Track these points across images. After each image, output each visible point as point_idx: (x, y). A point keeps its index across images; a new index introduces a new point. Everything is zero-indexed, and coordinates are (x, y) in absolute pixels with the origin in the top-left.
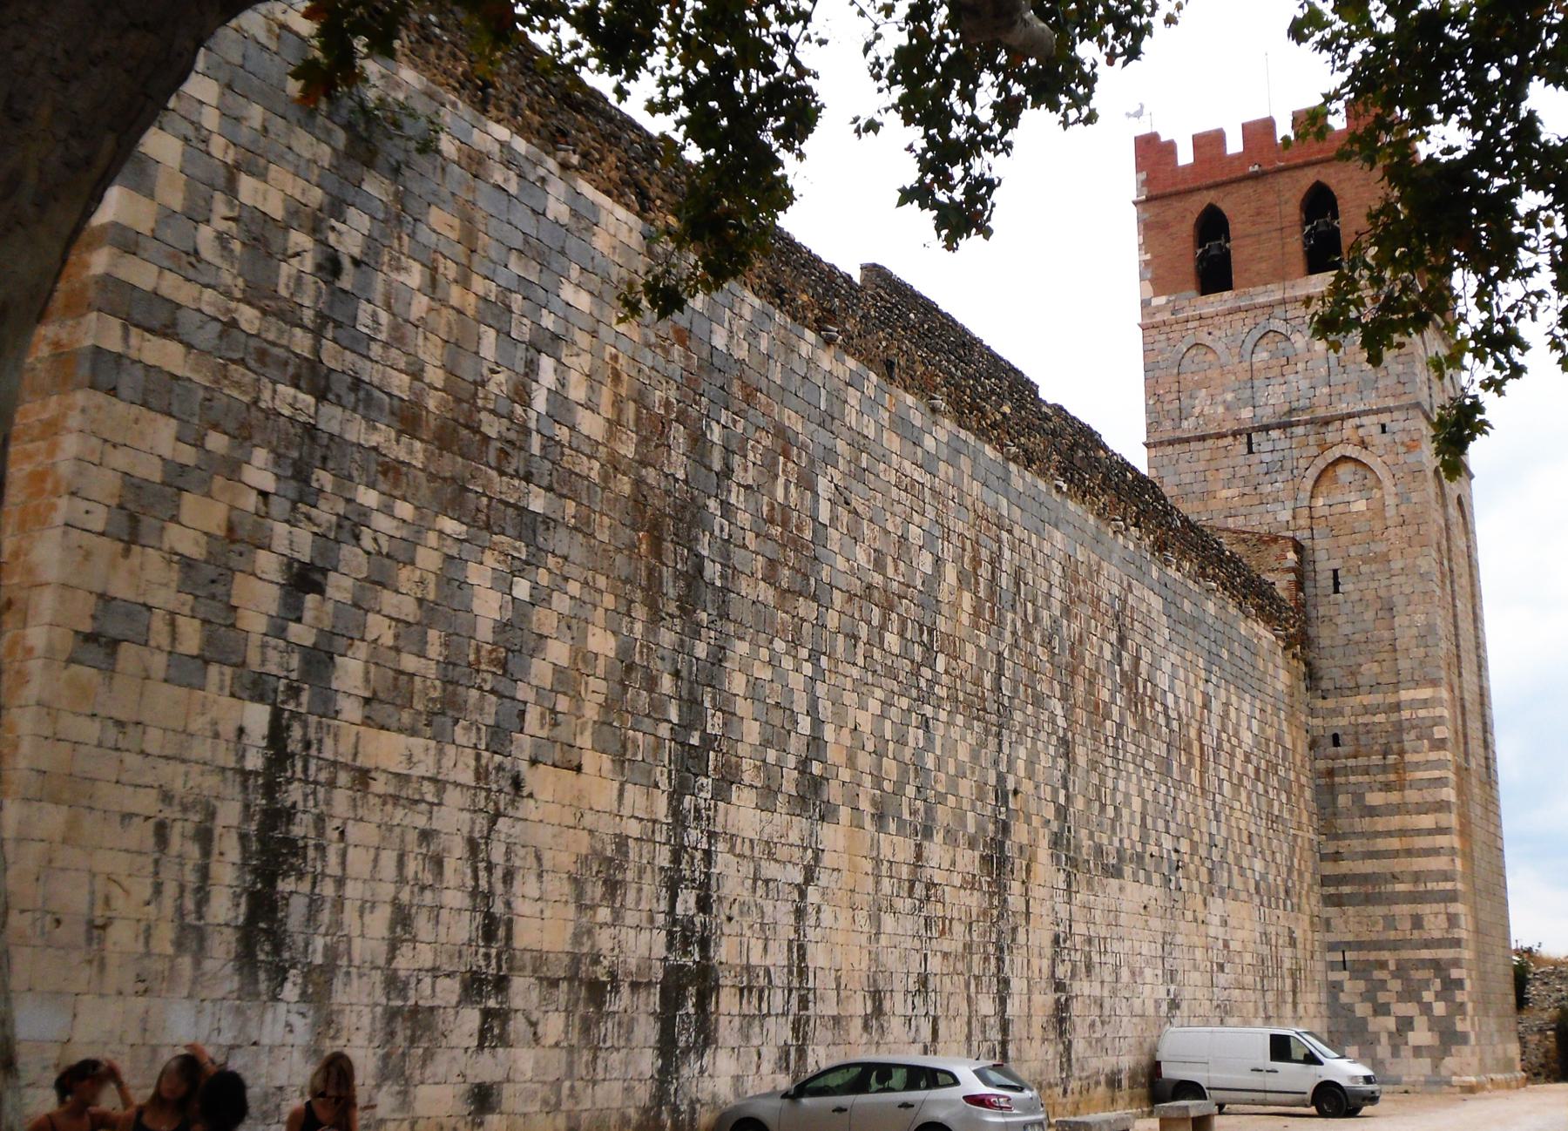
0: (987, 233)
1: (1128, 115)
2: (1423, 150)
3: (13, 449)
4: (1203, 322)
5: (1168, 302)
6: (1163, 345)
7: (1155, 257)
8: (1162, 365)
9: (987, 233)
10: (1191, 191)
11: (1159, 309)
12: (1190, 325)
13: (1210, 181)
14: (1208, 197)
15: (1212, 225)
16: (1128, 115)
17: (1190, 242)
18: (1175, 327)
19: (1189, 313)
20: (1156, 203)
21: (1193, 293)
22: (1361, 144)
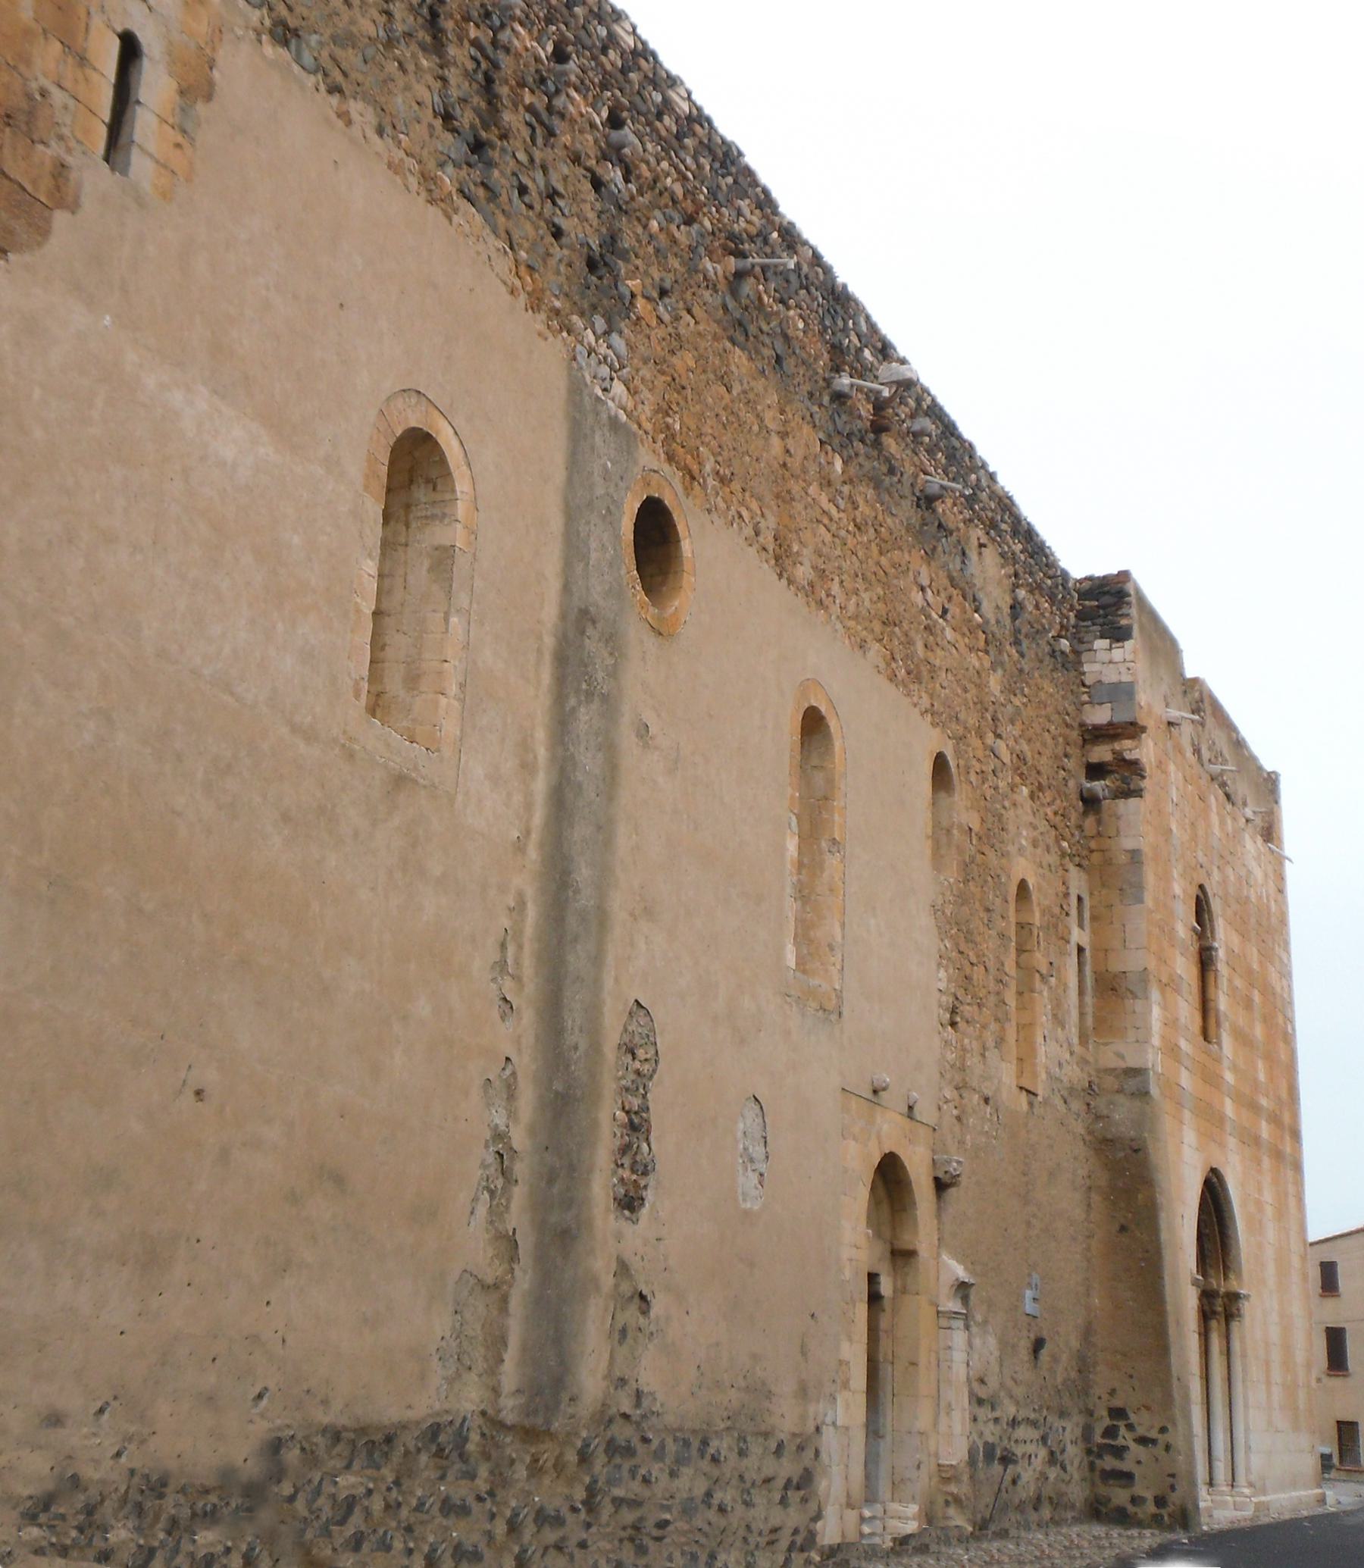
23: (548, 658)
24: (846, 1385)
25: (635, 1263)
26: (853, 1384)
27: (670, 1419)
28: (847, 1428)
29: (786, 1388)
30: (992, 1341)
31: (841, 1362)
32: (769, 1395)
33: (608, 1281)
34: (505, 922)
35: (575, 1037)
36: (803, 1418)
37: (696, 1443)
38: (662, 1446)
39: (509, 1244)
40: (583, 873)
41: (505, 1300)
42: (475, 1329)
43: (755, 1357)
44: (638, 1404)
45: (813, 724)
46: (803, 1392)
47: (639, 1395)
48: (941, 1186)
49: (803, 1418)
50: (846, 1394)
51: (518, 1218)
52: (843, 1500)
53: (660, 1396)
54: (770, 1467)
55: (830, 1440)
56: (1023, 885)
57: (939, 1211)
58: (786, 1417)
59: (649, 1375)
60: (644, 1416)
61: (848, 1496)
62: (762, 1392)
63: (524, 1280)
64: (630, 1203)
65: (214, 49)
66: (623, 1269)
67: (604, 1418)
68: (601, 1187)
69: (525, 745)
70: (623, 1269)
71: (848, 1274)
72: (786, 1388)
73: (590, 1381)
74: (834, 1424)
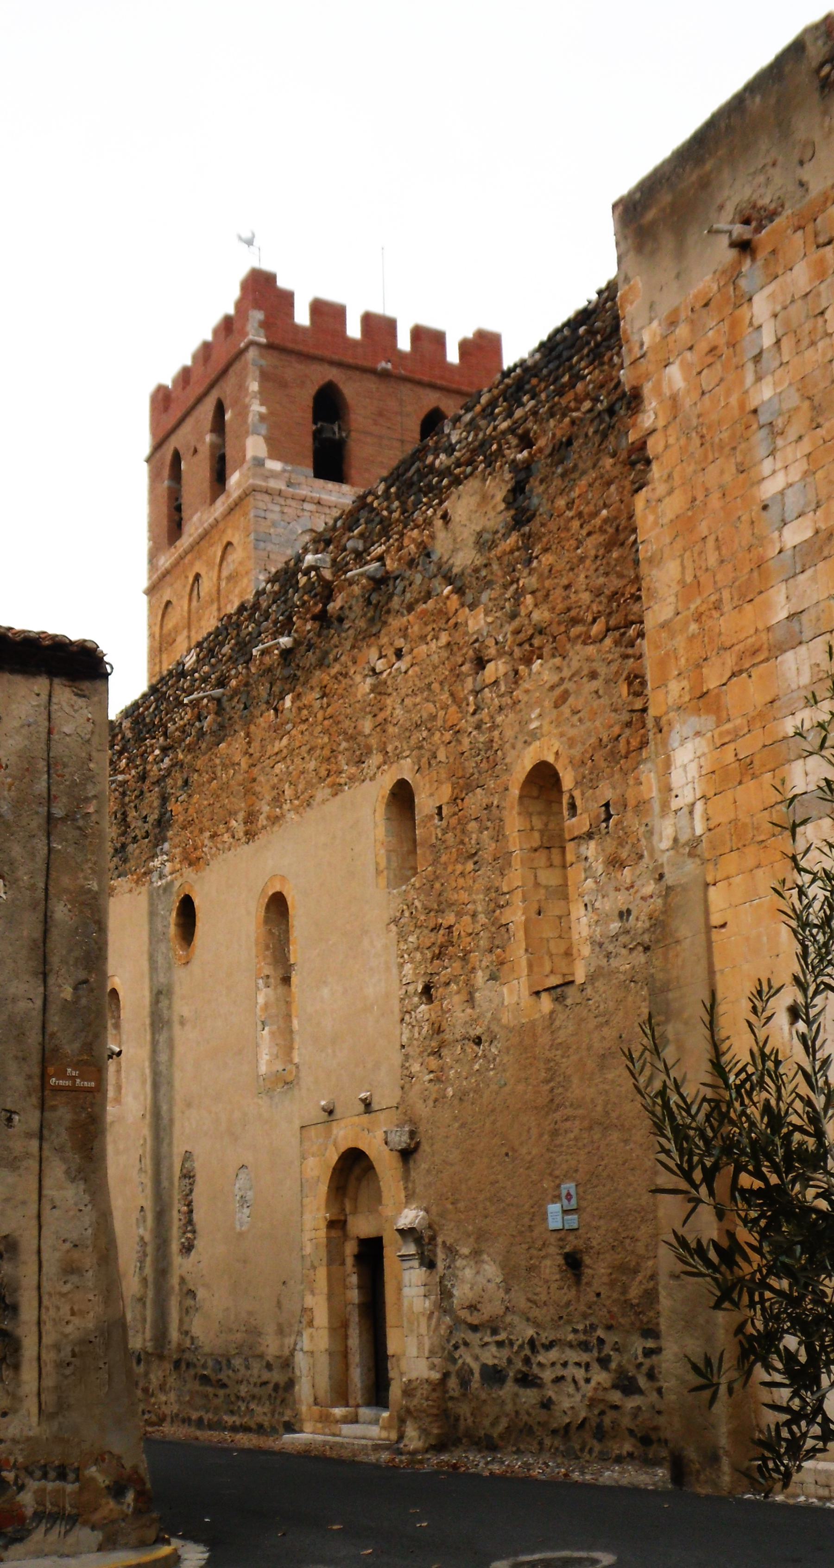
0: (261, 289)
1: (240, 238)
2: (253, 1246)
3: (831, 355)
4: (320, 509)
5: (284, 471)
6: (275, 517)
7: (271, 413)
8: (275, 539)
9: (261, 289)
10: (321, 360)
11: (273, 475)
12: (307, 506)
13: (336, 357)
14: (332, 374)
15: (328, 405)
16: (240, 238)
17: (309, 415)
18: (289, 502)
19: (304, 492)
20: (276, 353)
21: (310, 472)
22: (275, 597)
23: (148, 1028)
24: (310, 1324)
25: (188, 1278)
26: (316, 1323)
27: (207, 1349)
28: (312, 1353)
29: (270, 1329)
30: (491, 1270)
31: (304, 1310)
32: (260, 1334)
33: (177, 1287)
34: (141, 1152)
35: (165, 1184)
36: (282, 1346)
37: (224, 1362)
38: (206, 1362)
39: (144, 1280)
40: (165, 1108)
41: (144, 1304)
42: (138, 1317)
43: (250, 1313)
44: (192, 1343)
45: (278, 906)
46: (281, 1331)
47: (192, 1338)
48: (407, 1154)
49: (282, 1346)
50: (310, 1330)
51: (148, 1271)
52: (311, 1400)
53: (201, 1338)
54: (266, 1375)
55: (301, 1362)
56: (544, 779)
57: (406, 1176)
58: (271, 1346)
59: (197, 1327)
60: (196, 1348)
61: (315, 1399)
62: (255, 1332)
63: (150, 1294)
64: (188, 1248)
65: (77, 928)
66: (182, 1280)
67: (181, 1350)
68: (175, 1247)
69: (143, 1074)
70: (182, 1280)
71: (308, 1249)
72: (270, 1329)
73: (174, 1335)
74: (302, 1350)
